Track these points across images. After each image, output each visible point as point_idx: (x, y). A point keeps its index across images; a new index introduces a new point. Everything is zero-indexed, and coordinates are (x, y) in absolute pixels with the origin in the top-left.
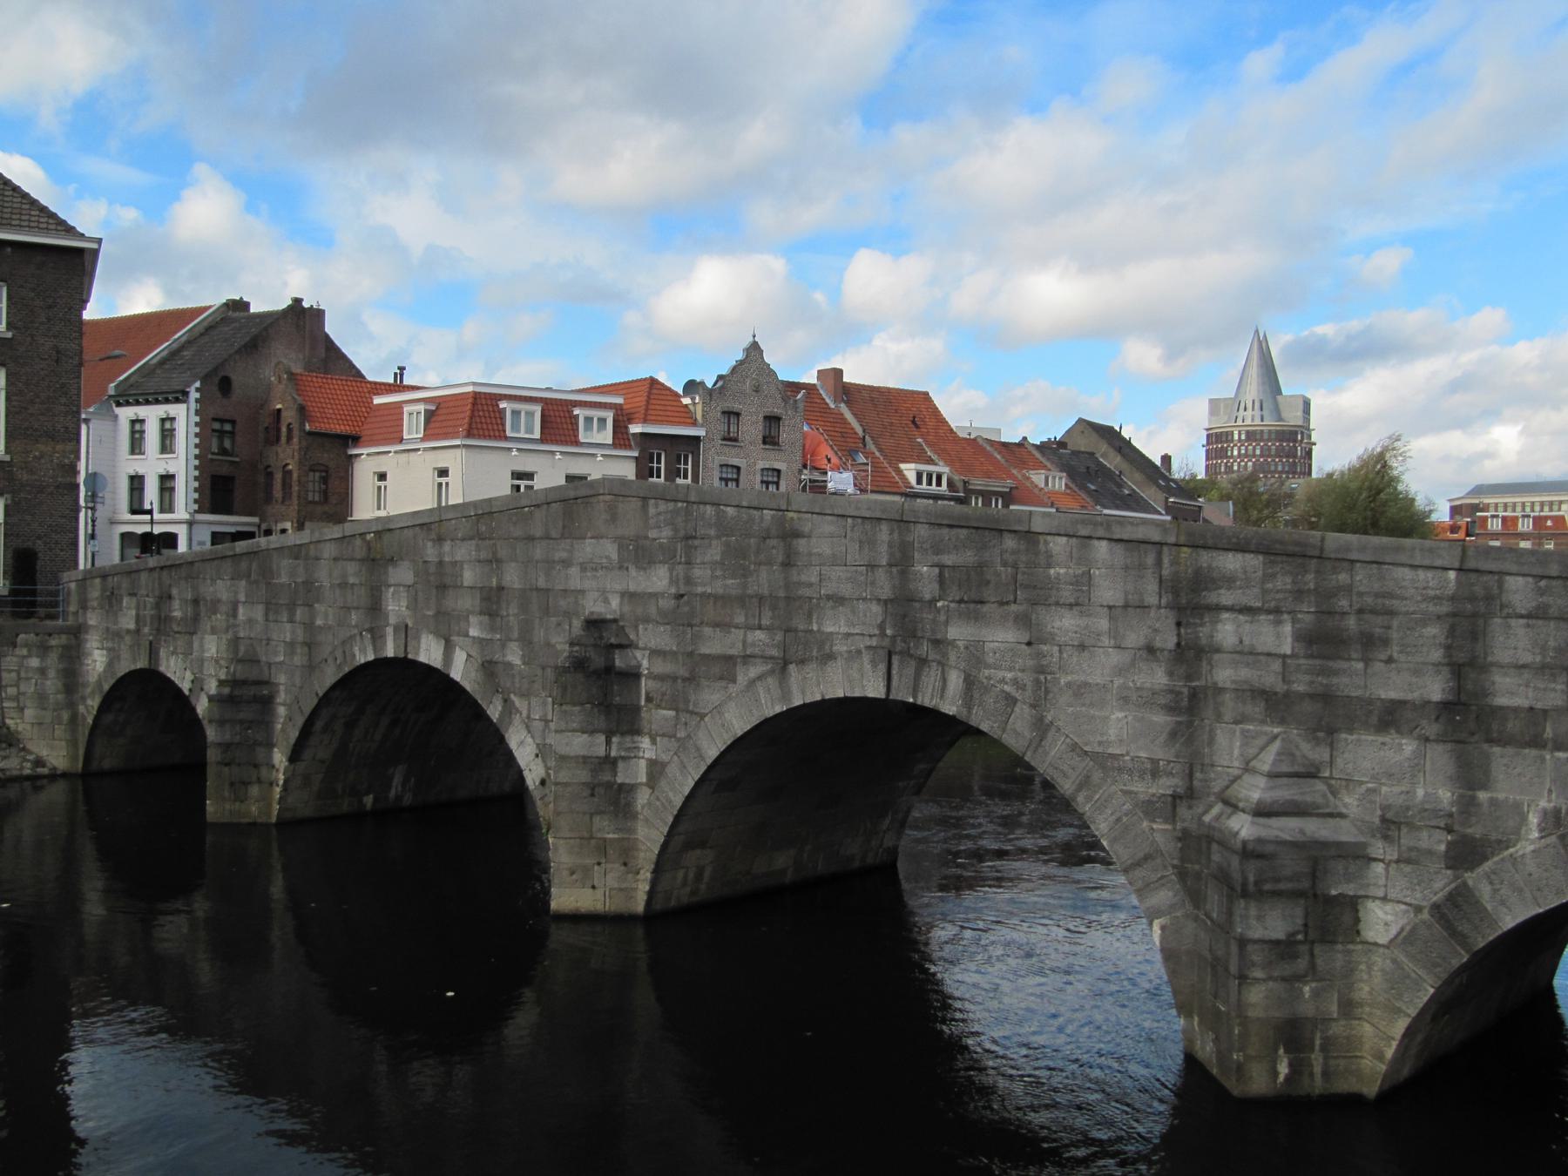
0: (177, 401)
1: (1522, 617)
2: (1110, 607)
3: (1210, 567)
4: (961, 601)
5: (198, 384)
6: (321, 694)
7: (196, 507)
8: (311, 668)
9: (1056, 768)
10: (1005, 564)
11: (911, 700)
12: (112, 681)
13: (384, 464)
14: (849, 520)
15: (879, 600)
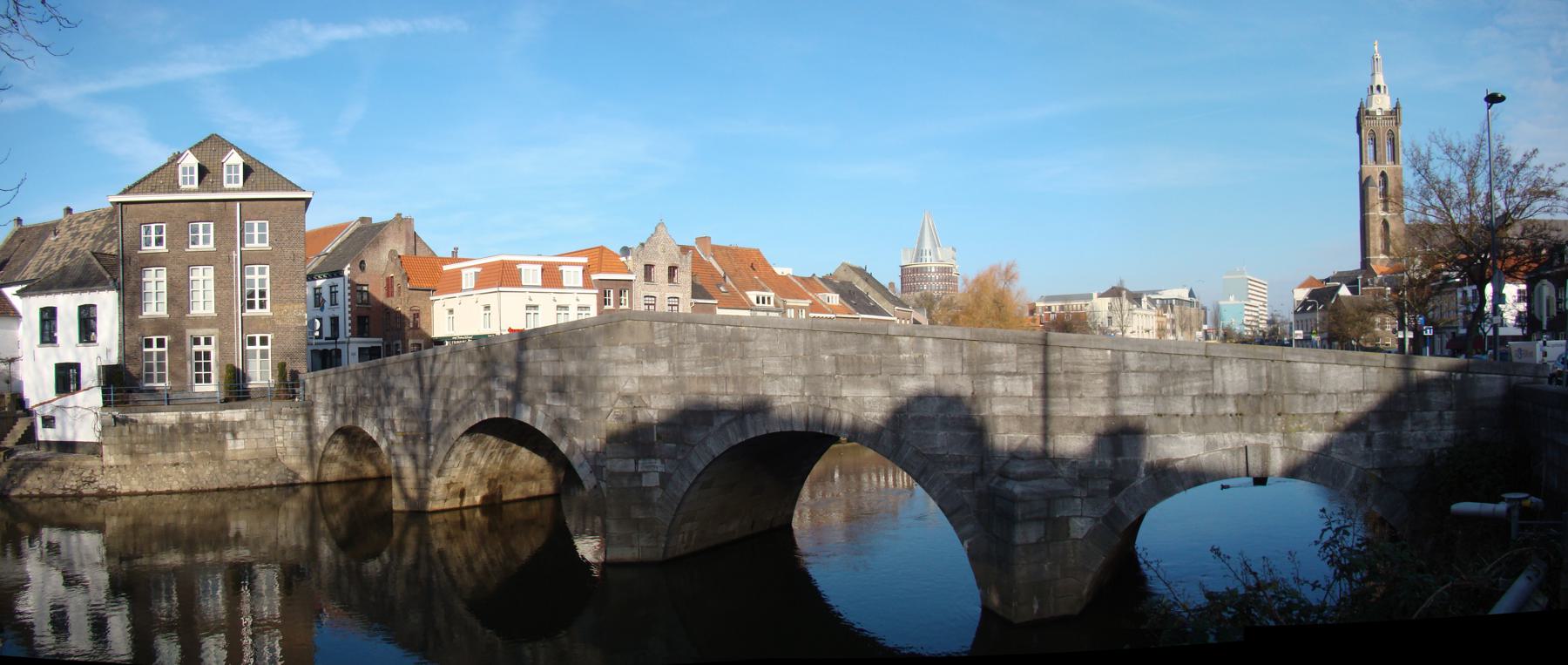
1: (1133, 372)
3: (989, 353)
4: (848, 375)
11: (821, 432)
13: (451, 304)
14: (779, 331)
15: (799, 376)
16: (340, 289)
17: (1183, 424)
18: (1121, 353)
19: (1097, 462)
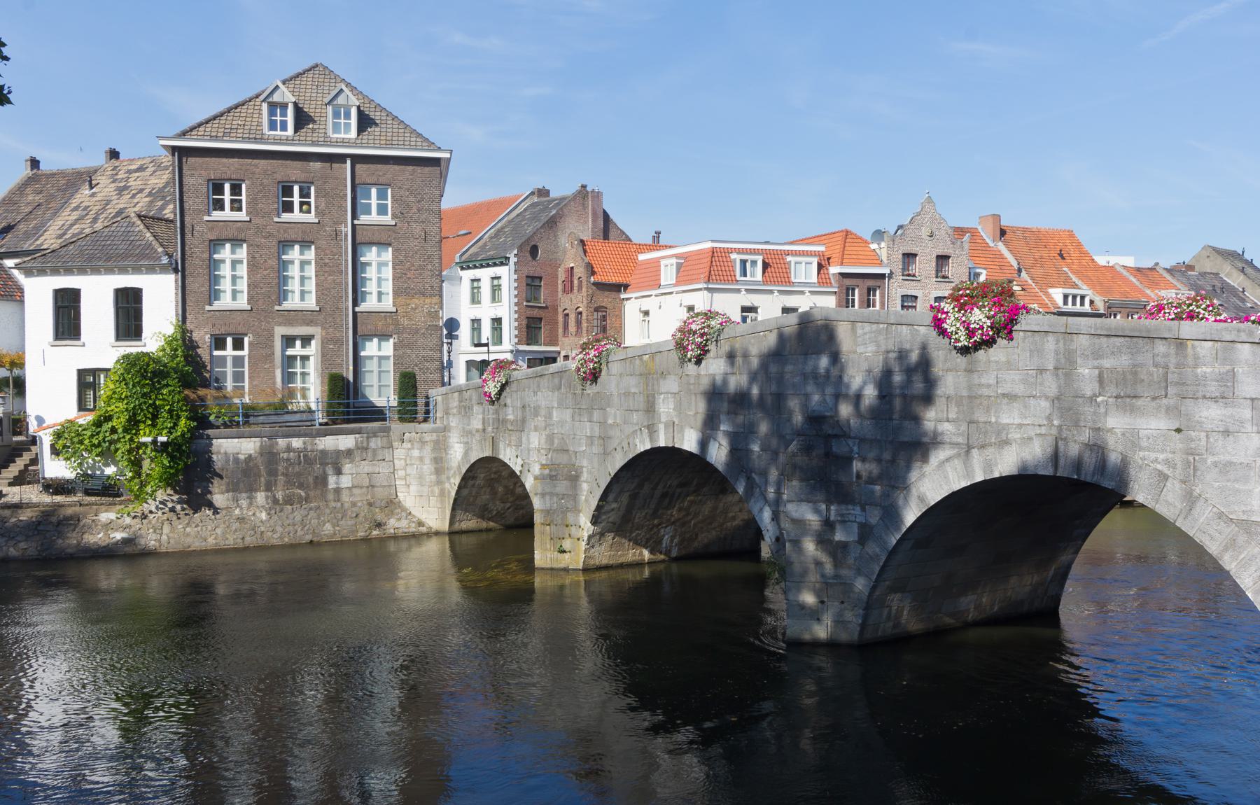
0: (502, 264)
2: (1252, 400)
5: (516, 252)
6: (612, 475)
7: (516, 340)
8: (606, 454)
9: (1204, 532)
10: (1156, 365)
11: (1076, 477)
12: (468, 466)
13: (646, 304)
16: (505, 283)
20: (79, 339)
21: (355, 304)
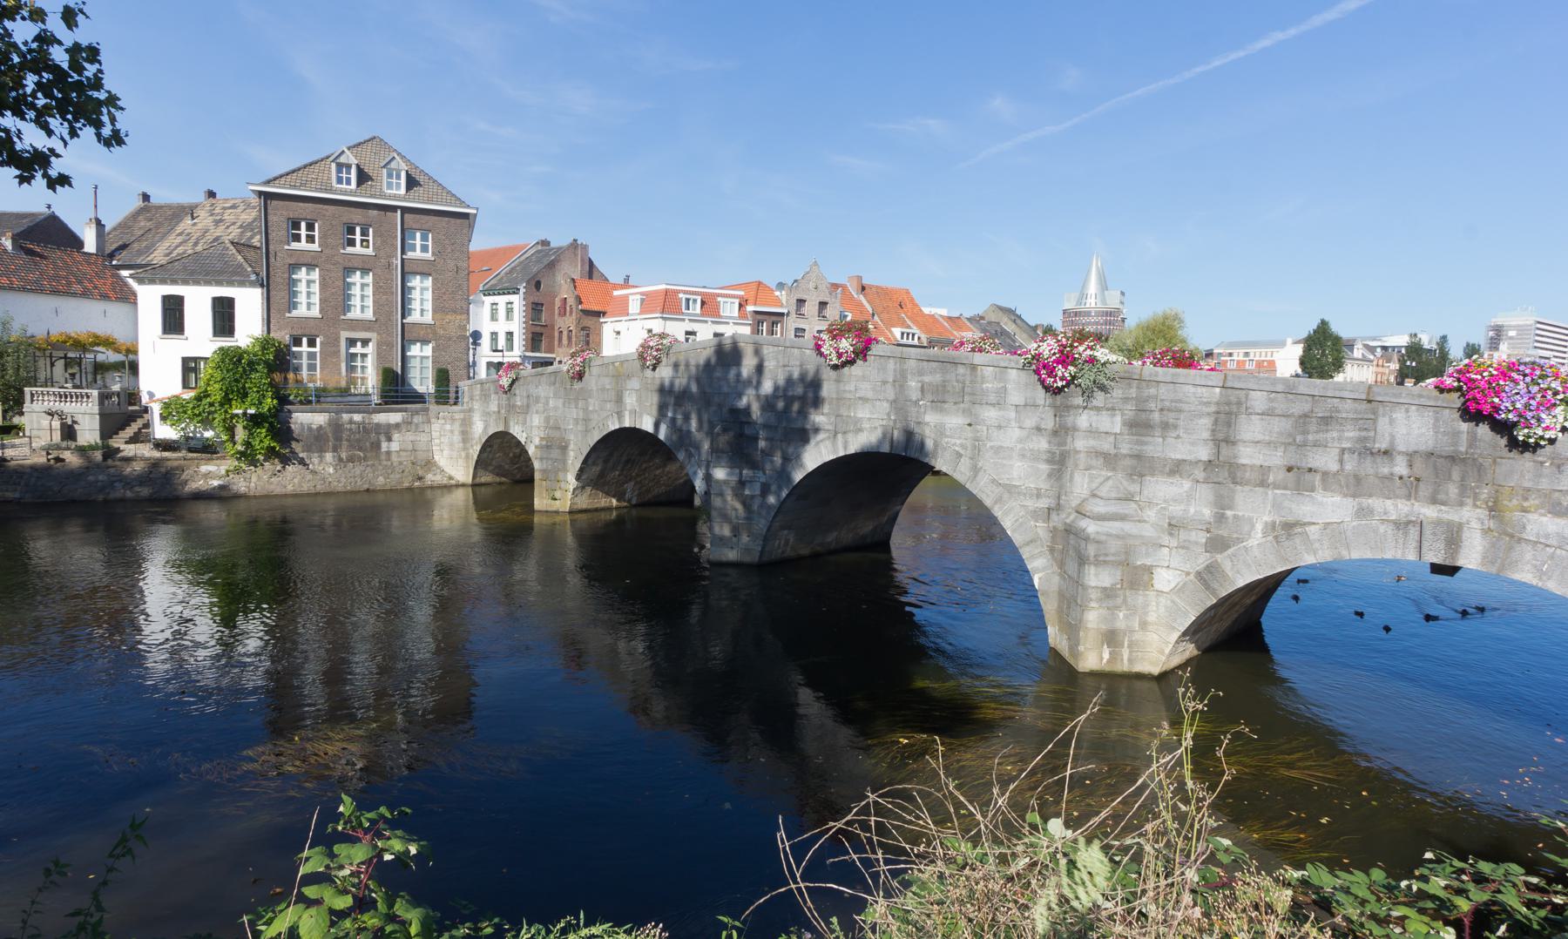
1: (1258, 414)
13: (618, 326)
17: (1323, 480)
18: (1244, 392)
19: (1192, 510)
20: (183, 334)
21: (403, 317)
